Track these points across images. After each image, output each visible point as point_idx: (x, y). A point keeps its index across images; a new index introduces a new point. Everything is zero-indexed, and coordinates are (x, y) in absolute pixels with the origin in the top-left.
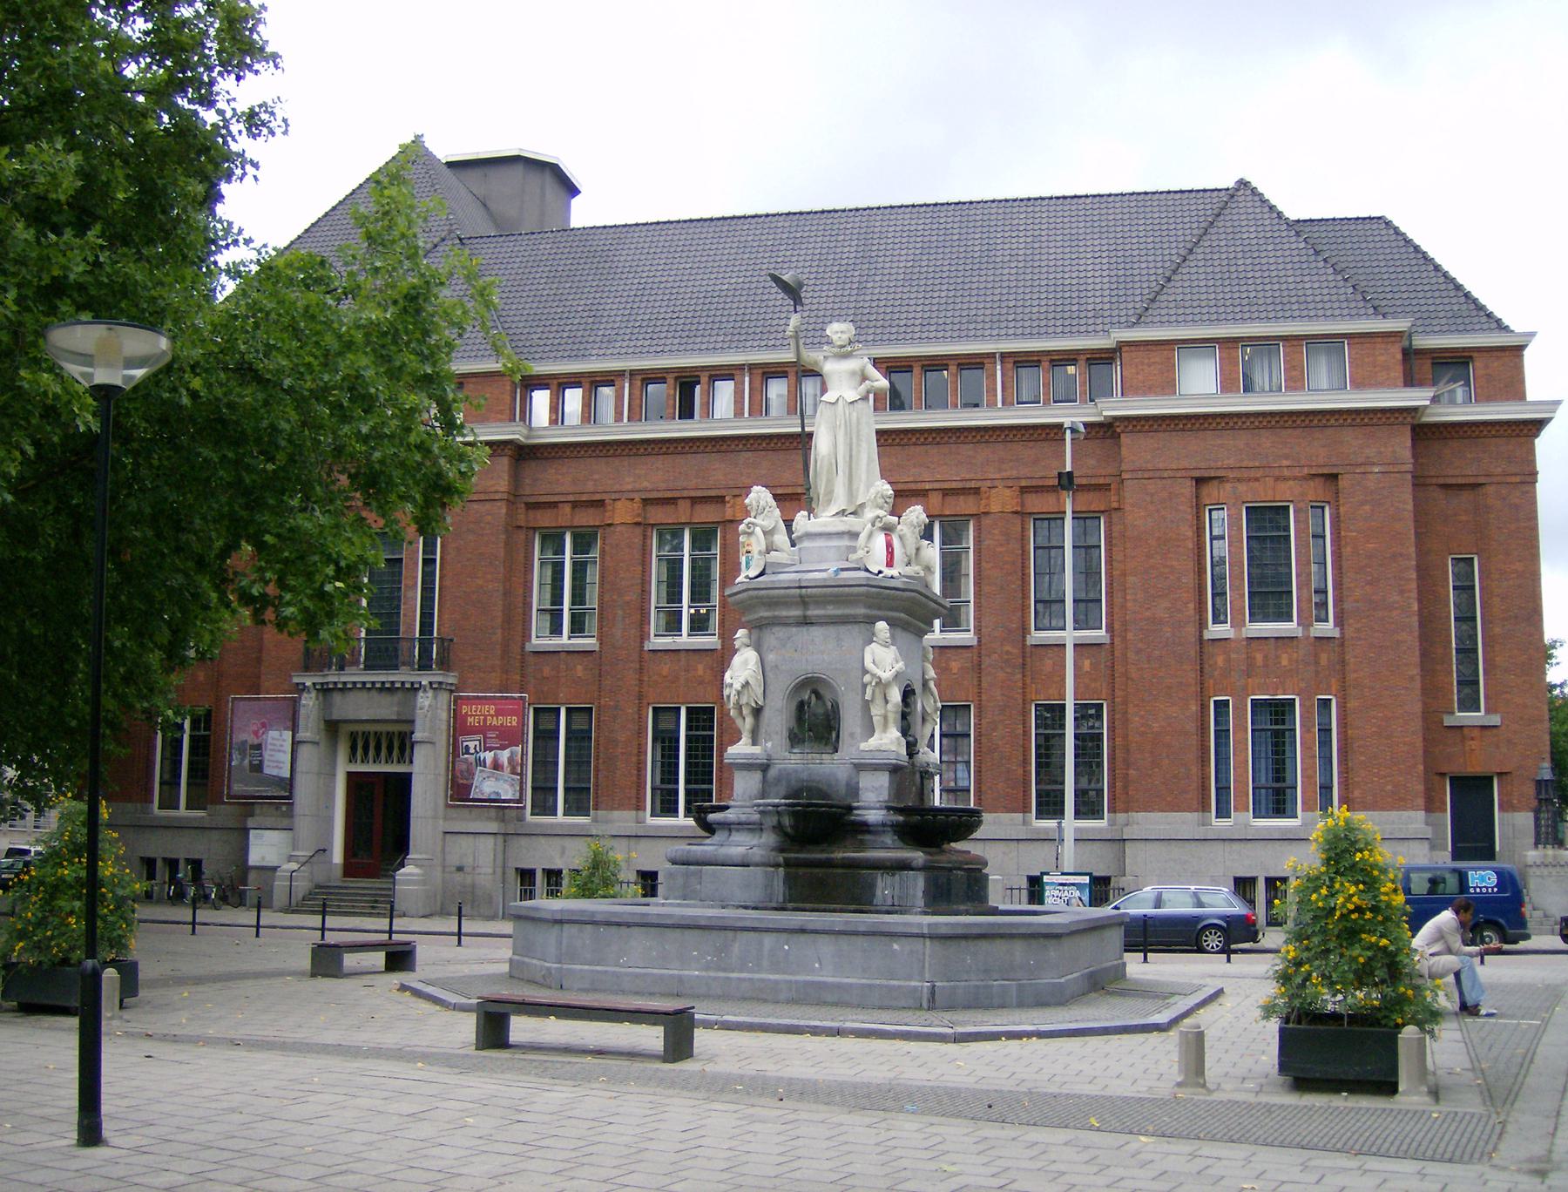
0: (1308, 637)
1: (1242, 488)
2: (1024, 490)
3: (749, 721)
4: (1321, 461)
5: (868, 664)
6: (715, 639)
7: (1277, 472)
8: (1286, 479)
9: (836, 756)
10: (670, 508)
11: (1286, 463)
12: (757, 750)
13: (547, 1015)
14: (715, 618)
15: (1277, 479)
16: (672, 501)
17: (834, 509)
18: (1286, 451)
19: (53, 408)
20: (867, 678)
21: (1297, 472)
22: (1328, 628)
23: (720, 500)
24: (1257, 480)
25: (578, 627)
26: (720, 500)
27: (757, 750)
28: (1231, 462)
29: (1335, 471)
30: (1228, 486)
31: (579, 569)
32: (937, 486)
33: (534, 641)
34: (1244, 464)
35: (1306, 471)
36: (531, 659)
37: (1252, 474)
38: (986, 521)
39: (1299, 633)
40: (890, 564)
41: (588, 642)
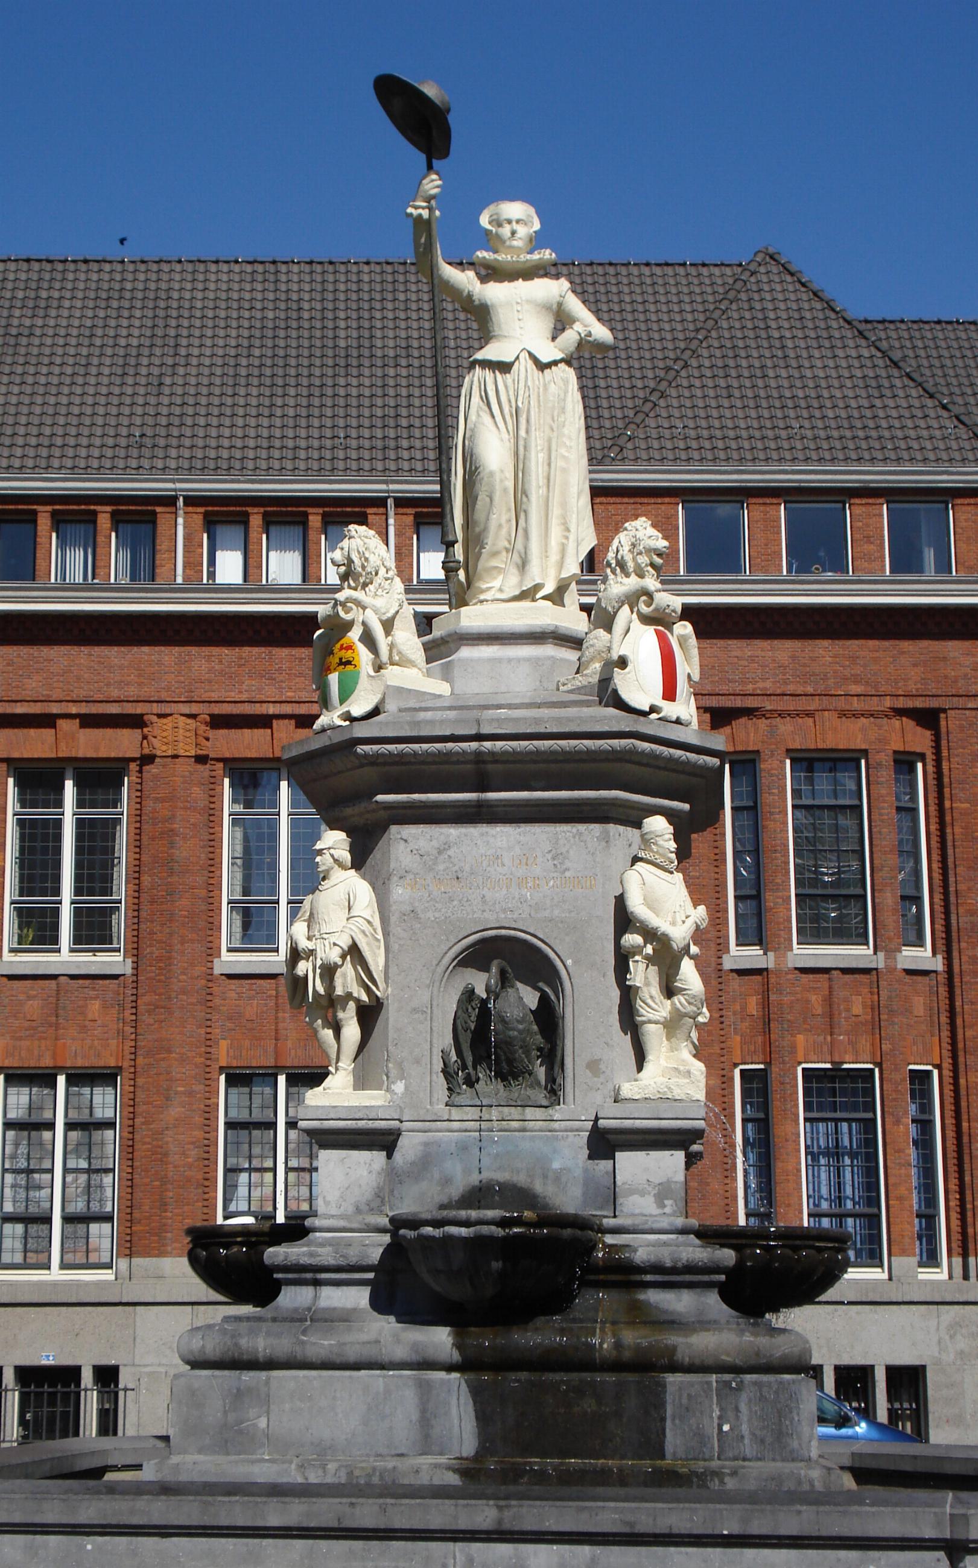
0: (891, 970)
1: (785, 727)
2: (219, 722)
3: (352, 1031)
4: (912, 688)
5: (636, 905)
6: (118, 958)
7: (842, 704)
8: (856, 715)
9: (557, 1112)
10: (47, 733)
11: (855, 689)
12: (373, 1099)
13: (341, 1364)
14: (120, 923)
15: (843, 714)
16: (47, 721)
17: (512, 584)
18: (858, 670)
19: (420, 523)
20: (632, 939)
21: (873, 704)
22: (922, 956)
23: (136, 722)
24: (809, 714)
25: (93, 930)
26: (136, 722)
27: (373, 1099)
28: (768, 685)
29: (934, 703)
30: (762, 723)
31: (95, 840)
32: (287, 709)
33: (225, 956)
34: (791, 688)
35: (888, 702)
36: (736, 982)
37: (802, 704)
38: (151, 770)
39: (880, 961)
40: (670, 694)
41: (112, 961)
